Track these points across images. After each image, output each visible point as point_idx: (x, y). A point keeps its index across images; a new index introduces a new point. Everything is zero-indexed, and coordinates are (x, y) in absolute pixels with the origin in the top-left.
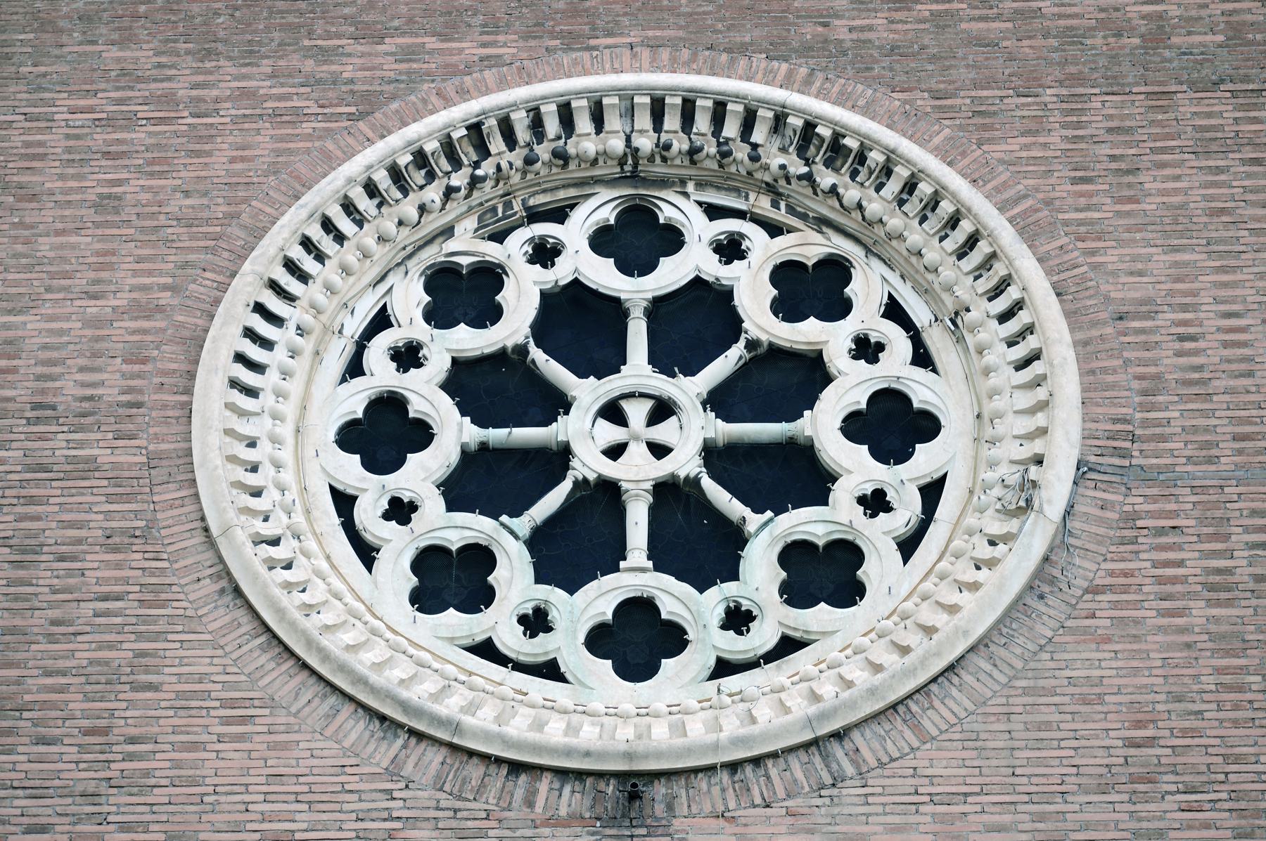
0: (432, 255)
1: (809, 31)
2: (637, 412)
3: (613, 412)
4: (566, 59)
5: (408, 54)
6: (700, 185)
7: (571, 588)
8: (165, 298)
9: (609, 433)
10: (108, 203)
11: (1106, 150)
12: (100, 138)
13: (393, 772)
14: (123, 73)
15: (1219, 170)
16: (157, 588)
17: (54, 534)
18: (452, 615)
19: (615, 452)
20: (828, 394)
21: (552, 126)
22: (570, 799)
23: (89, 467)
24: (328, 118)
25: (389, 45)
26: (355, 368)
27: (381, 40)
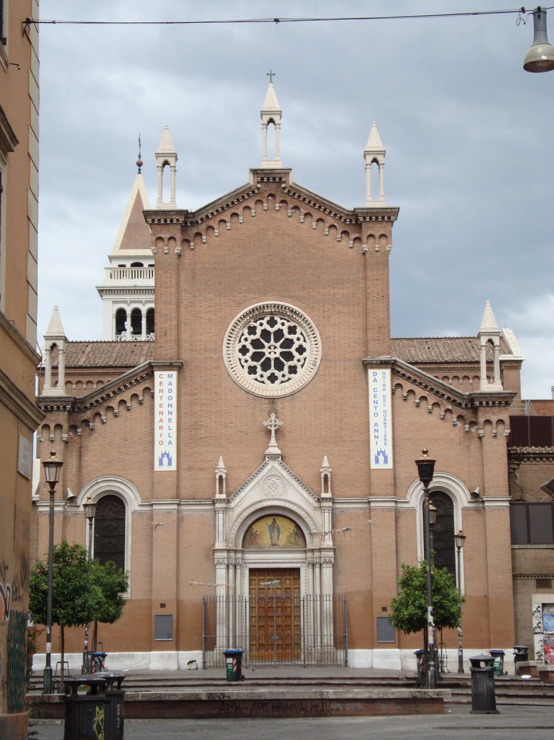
0: (248, 325)
1: (293, 294)
2: (272, 348)
3: (270, 348)
4: (264, 298)
5: (244, 296)
6: (280, 315)
7: (265, 371)
8: (218, 334)
9: (269, 350)
10: (210, 319)
11: (327, 313)
12: (208, 309)
13: (248, 398)
14: (210, 299)
15: (339, 317)
16: (221, 374)
17: (209, 367)
18: (247, 354)
19: (270, 353)
20: (294, 346)
21: (262, 309)
22: (267, 401)
23: (211, 358)
24: (236, 306)
25: (243, 295)
26: (240, 341)
27: (241, 294)
